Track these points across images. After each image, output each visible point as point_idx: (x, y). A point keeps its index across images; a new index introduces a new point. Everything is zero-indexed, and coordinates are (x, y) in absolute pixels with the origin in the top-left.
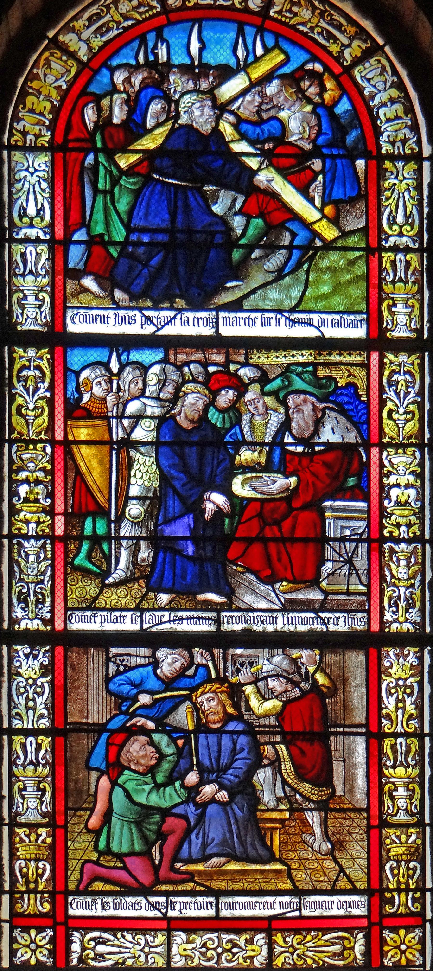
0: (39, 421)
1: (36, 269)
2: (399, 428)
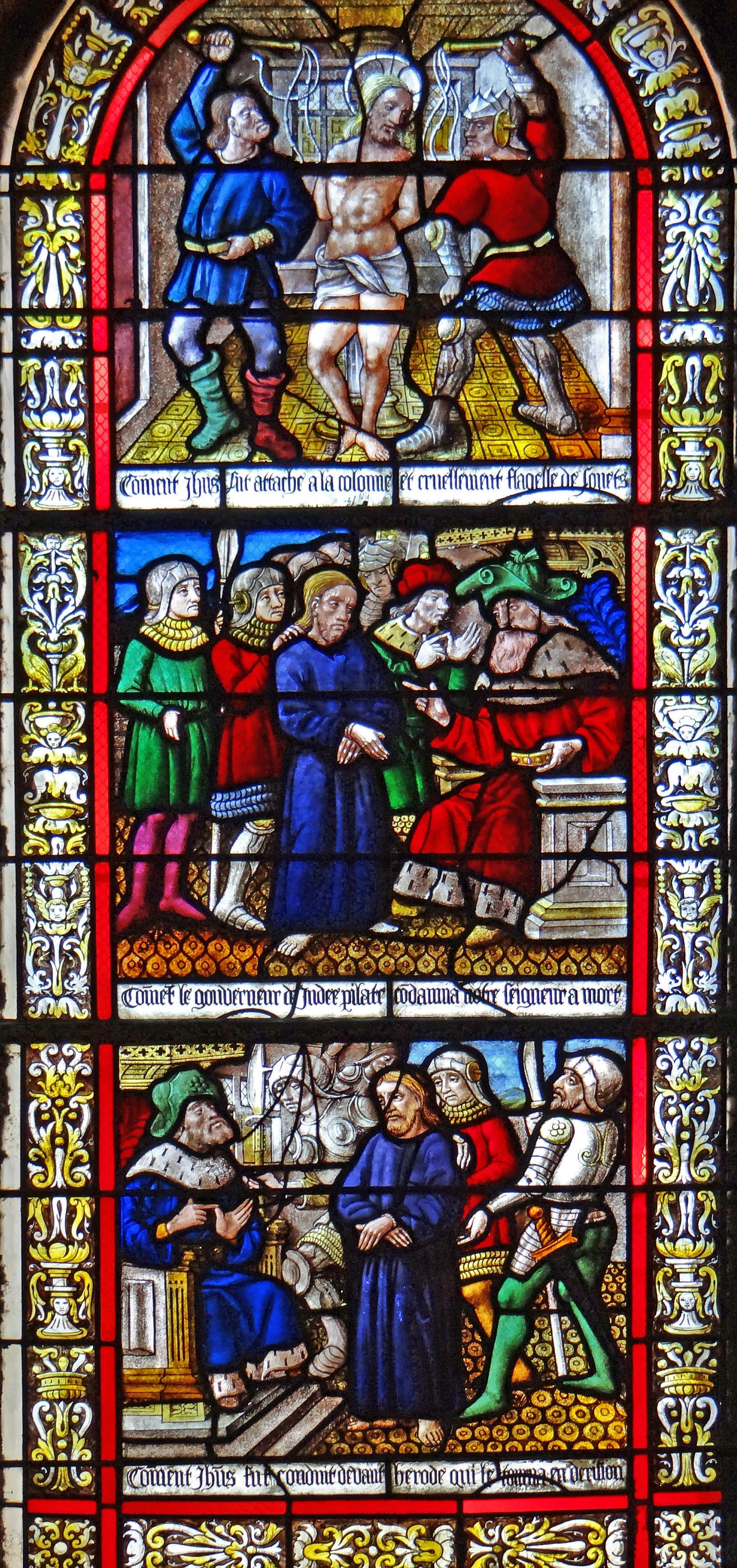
0: (700, 655)
1: (62, 399)
2: (682, 660)
